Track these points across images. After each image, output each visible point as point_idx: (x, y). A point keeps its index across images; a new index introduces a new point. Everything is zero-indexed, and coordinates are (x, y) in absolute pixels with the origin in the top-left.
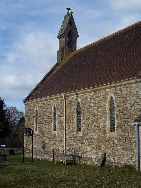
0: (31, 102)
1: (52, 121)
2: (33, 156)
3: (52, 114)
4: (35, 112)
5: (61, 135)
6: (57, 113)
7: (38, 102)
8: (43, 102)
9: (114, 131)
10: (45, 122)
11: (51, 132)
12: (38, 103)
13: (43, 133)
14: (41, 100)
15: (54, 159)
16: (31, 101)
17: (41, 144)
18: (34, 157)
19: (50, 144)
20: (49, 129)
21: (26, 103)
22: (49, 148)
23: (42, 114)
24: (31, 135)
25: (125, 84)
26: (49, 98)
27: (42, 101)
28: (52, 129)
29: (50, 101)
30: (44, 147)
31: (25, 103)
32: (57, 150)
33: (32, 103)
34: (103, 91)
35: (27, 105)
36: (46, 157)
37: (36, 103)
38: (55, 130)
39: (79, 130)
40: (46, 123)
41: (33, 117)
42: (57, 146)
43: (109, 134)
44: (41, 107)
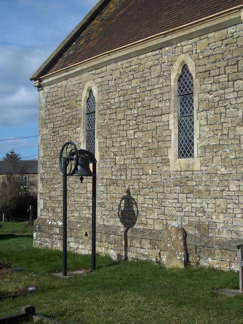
0: (64, 75)
1: (172, 122)
2: (129, 253)
3: (173, 96)
4: (83, 104)
5: (223, 170)
6: (196, 90)
7: (96, 67)
8: (119, 63)
9: (191, 156)
10: (132, 132)
11: (166, 162)
12: (98, 71)
13: (124, 168)
14: (113, 56)
15: (187, 262)
16: (67, 70)
17: (117, 207)
18: (131, 255)
19: (161, 205)
20: (157, 152)
21: (45, 81)
22: (148, 219)
23: (117, 105)
24: (88, 173)
25: (78, 72)
26: (107, 58)
27: (116, 60)
28: (173, 151)
29: (157, 52)
30: (128, 215)
31: (41, 81)
32: (204, 228)
33: (66, 78)
34: (64, 83)
35: (46, 89)
36: (142, 251)
37: (85, 75)
38: (186, 150)
39: (186, 150)
40: (139, 134)
41: (74, 121)
42: (205, 212)
43: (176, 163)
44: (112, 83)
